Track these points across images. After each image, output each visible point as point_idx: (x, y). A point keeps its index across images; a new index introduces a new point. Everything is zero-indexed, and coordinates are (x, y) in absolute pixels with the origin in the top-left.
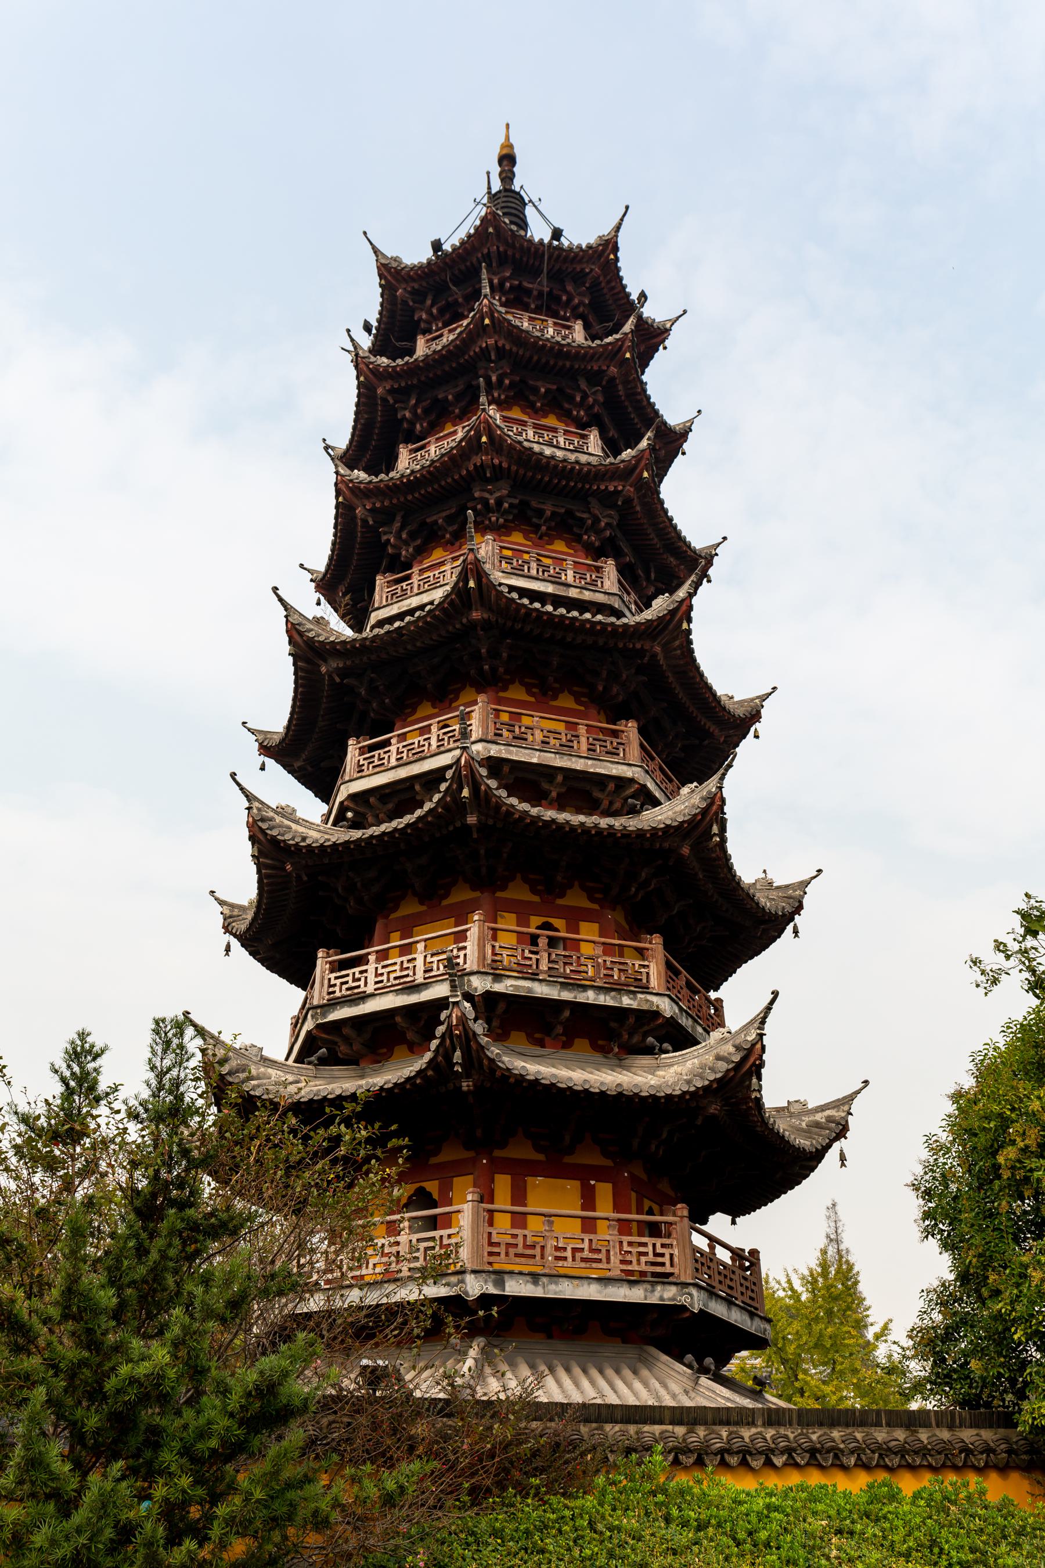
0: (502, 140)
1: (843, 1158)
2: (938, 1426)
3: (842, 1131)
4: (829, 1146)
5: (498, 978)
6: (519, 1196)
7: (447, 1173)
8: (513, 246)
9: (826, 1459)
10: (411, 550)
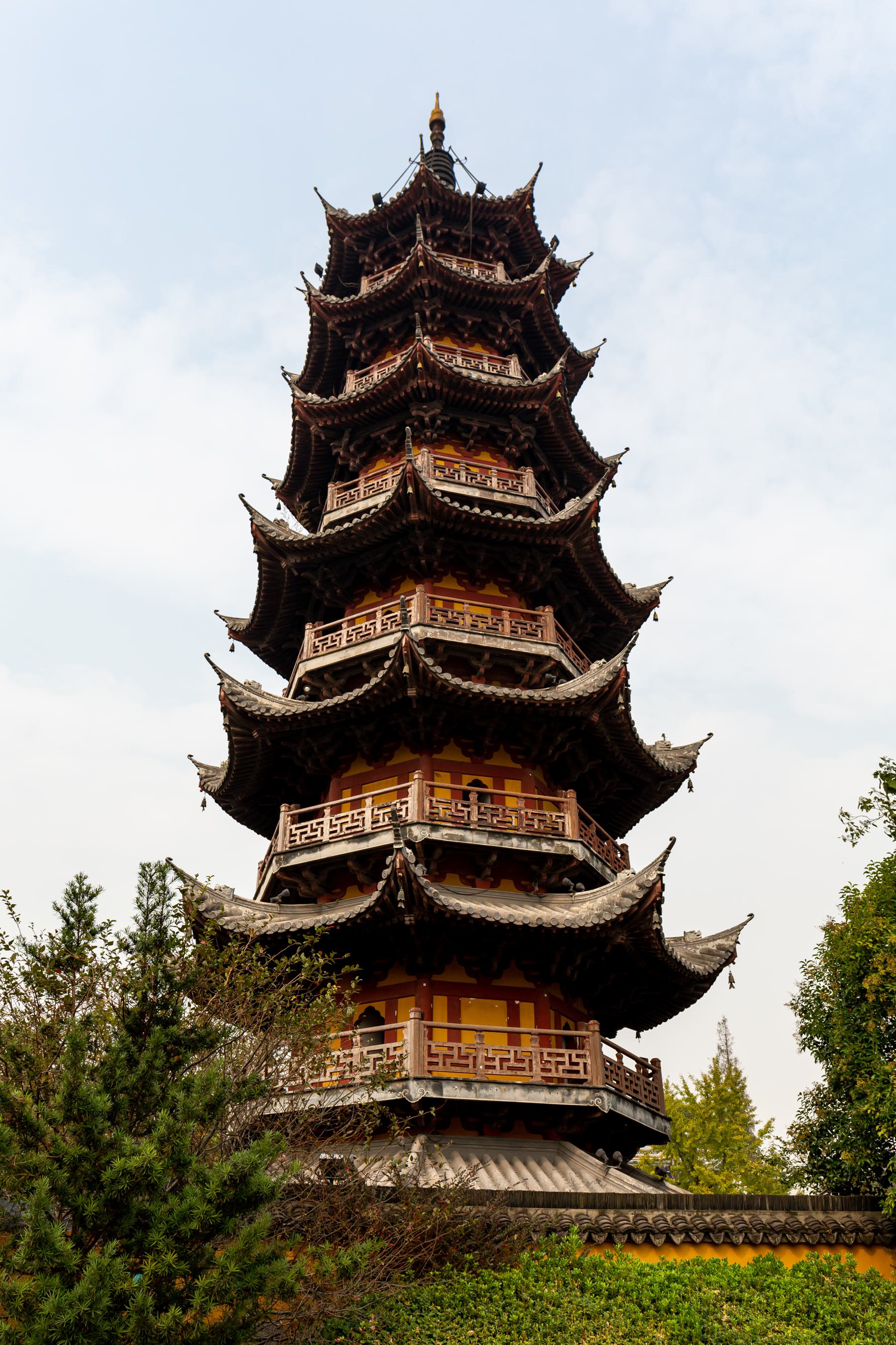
0: (433, 107)
1: (731, 981)
2: (814, 1209)
4: (719, 970)
5: (435, 828)
6: (454, 1014)
7: (393, 995)
8: (443, 199)
9: (718, 1238)
10: (358, 461)
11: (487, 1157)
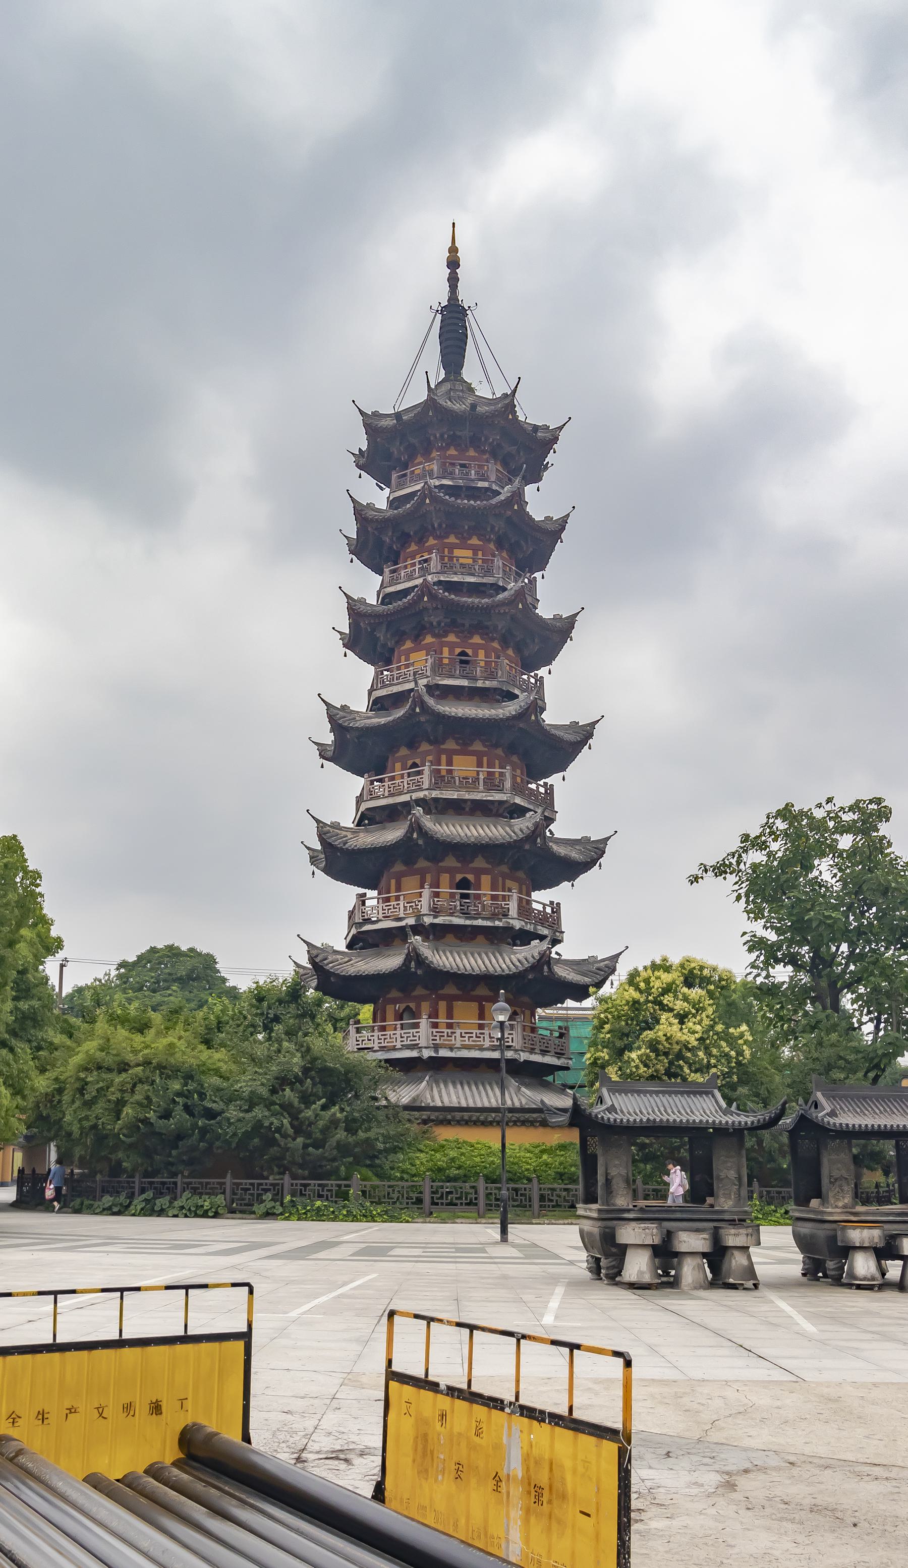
3: (590, 735)
5: (435, 917)
11: (465, 1082)
